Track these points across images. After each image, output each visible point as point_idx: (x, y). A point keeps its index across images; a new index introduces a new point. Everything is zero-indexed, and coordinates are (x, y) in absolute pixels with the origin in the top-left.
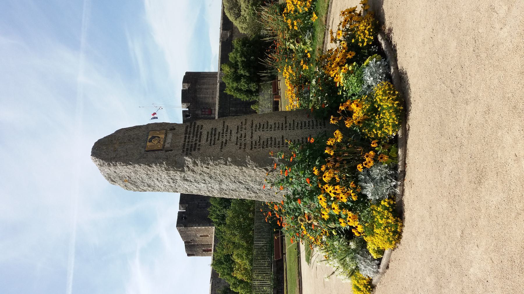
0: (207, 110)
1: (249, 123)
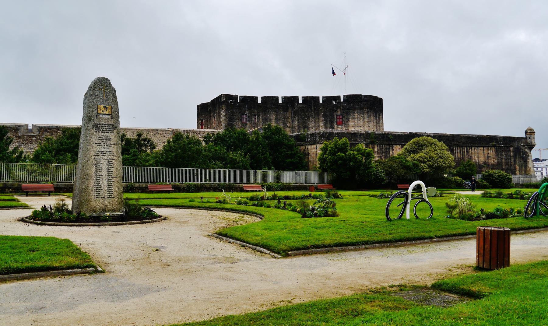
0: (341, 120)
1: (113, 158)
